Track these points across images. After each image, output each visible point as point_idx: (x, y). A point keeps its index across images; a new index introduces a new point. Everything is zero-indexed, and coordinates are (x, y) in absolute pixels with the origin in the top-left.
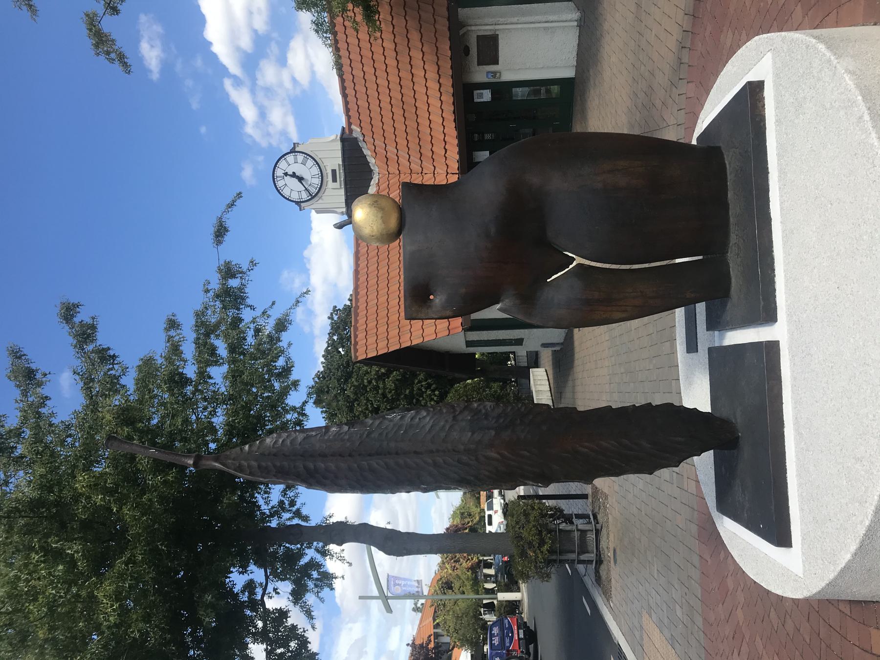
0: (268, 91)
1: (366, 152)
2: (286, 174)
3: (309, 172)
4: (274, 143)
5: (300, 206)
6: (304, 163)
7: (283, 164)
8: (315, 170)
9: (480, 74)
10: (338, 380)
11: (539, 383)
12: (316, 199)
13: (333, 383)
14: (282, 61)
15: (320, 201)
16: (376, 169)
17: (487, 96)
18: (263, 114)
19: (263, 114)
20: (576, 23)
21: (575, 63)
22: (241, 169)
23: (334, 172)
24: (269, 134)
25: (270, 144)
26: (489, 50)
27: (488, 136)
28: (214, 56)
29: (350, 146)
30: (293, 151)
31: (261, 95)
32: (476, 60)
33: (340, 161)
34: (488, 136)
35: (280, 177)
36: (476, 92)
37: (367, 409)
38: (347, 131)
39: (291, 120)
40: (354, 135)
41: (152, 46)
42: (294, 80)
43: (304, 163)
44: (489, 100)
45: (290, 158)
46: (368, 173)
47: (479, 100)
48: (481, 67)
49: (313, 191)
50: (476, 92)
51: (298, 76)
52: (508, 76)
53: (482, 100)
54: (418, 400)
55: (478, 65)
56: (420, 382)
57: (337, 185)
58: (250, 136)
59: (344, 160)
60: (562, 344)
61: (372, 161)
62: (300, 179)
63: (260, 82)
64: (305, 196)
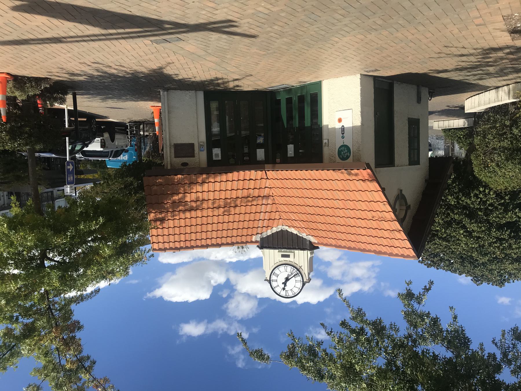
0: (343, 274)
1: (269, 233)
2: (284, 289)
3: (283, 273)
4: (374, 275)
5: (306, 282)
6: (277, 276)
7: (278, 290)
8: (282, 268)
9: (201, 157)
10: (475, 267)
11: (473, 105)
12: (301, 270)
13: (478, 272)
14: (329, 264)
16: (280, 228)
17: (217, 152)
18: (357, 279)
19: (357, 279)
20: (165, 93)
21: (194, 91)
22: (190, 338)
23: (283, 256)
24: (369, 278)
26: (185, 150)
27: (246, 150)
28: (326, 300)
29: (266, 243)
30: (270, 282)
31: (346, 279)
32: (191, 158)
33: (276, 251)
34: (246, 150)
35: (286, 293)
36: (214, 158)
37: (498, 248)
38: (258, 244)
39: (361, 264)
40: (259, 239)
41: (319, 333)
42: (339, 259)
43: (277, 276)
44: (220, 149)
45: (274, 284)
46: (283, 233)
47: (220, 156)
48: (196, 155)
49: (295, 271)
50: (214, 158)
51: (337, 257)
52: (203, 138)
53: (220, 155)
54: (489, 205)
55: (193, 156)
56: (472, 203)
57: (292, 255)
60: (418, 86)
61: (275, 230)
62: (287, 279)
63: (339, 278)
64: (299, 278)
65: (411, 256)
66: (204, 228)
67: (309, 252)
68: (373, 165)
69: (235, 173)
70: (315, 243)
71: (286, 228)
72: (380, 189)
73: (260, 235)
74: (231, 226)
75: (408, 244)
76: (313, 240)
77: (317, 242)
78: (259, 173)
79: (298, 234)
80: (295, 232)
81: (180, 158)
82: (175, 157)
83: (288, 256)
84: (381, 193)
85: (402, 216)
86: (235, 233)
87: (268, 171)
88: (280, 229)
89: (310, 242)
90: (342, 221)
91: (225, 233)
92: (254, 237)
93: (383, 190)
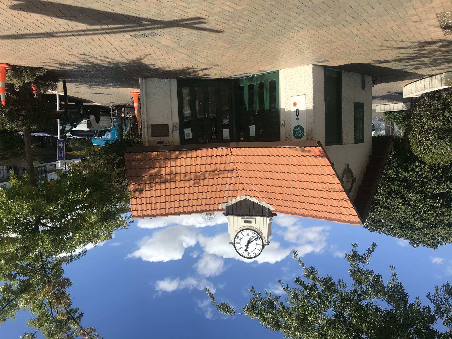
0: (298, 238)
1: (234, 202)
2: (246, 250)
3: (246, 236)
4: (324, 238)
5: (266, 245)
6: (241, 239)
7: (241, 251)
8: (245, 232)
9: (175, 136)
10: (412, 231)
11: (410, 91)
12: (261, 234)
13: (414, 235)
14: (285, 229)
15: (262, 232)
16: (243, 198)
17: (188, 132)
18: (310, 242)
19: (310, 242)
20: (144, 80)
21: (168, 79)
22: (165, 293)
23: (245, 222)
24: (320, 241)
25: (325, 241)
26: (160, 130)
27: (213, 130)
28: (283, 260)
29: (231, 211)
30: (234, 244)
31: (300, 242)
32: (166, 137)
33: (240, 218)
34: (213, 130)
35: (248, 254)
36: (186, 137)
37: (432, 215)
39: (314, 229)
40: (224, 208)
41: (277, 289)
42: (294, 225)
43: (241, 239)
44: (190, 129)
45: (238, 246)
46: (245, 202)
47: (191, 136)
49: (256, 235)
50: (186, 137)
51: (292, 223)
52: (176, 119)
53: (191, 134)
54: (425, 178)
56: (410, 176)
57: (253, 221)
58: (321, 250)
59: (238, 215)
60: (363, 75)
61: (238, 199)
62: (249, 242)
63: (294, 241)
64: (259, 241)
65: (357, 222)
66: (177, 198)
67: (268, 218)
68: (323, 143)
69: (204, 150)
70: (273, 211)
71: (248, 198)
72: (329, 164)
73: (225, 204)
74: (200, 196)
75: (354, 212)
76: (271, 208)
77: (275, 210)
78: (225, 150)
79: (259, 203)
80: (256, 201)
81: (156, 137)
82: (152, 136)
83: (250, 222)
84: (330, 167)
85: (349, 187)
86: (204, 202)
87: (233, 148)
88: (243, 199)
89: (269, 210)
90: (296, 192)
91: (195, 202)
92: (220, 205)
93: (332, 165)
